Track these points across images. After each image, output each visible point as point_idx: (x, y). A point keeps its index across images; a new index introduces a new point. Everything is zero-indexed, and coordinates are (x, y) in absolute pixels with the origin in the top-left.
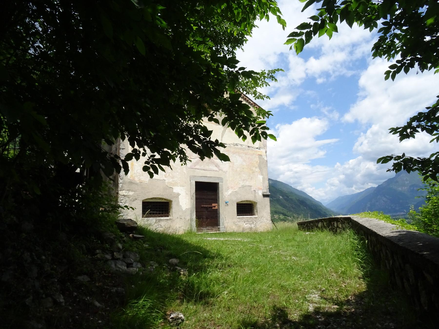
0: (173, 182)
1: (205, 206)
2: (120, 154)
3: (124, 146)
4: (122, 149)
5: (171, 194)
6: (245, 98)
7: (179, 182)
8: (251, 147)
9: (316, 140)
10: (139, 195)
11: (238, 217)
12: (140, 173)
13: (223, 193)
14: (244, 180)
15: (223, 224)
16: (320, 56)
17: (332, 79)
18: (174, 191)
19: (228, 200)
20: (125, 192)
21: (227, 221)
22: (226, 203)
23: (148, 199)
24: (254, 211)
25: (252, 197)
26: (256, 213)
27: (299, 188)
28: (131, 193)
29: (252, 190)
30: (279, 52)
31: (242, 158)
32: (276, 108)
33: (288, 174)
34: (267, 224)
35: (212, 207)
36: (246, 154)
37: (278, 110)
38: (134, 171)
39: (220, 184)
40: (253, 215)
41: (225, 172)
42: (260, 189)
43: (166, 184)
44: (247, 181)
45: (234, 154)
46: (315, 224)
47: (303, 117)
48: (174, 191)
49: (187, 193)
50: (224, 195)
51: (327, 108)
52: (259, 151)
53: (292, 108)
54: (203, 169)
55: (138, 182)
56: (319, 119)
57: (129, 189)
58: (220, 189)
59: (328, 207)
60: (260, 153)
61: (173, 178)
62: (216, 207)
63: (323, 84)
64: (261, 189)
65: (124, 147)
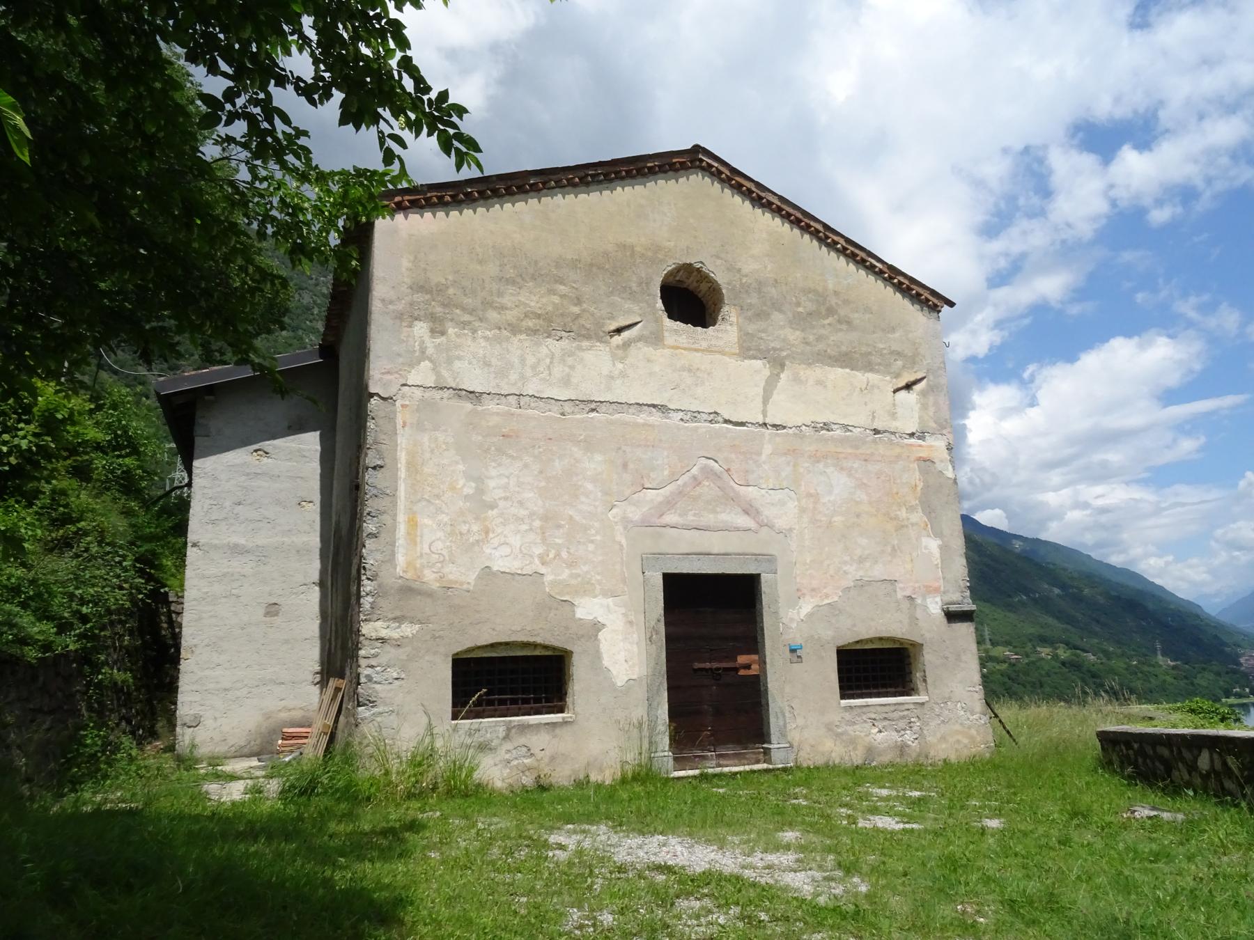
0: (573, 582)
1: (708, 665)
2: (367, 487)
3: (379, 459)
4: (374, 468)
5: (567, 628)
6: (852, 252)
7: (599, 577)
8: (885, 431)
9: (1165, 406)
10: (439, 637)
11: (844, 702)
12: (445, 552)
13: (776, 613)
14: (861, 560)
15: (783, 735)
16: (1155, 138)
17: (1204, 204)
18: (580, 613)
19: (799, 641)
20: (385, 625)
21: (800, 721)
22: (793, 651)
23: (479, 648)
24: (914, 679)
25: (901, 622)
26: (920, 685)
27: (1116, 560)
28: (408, 630)
29: (900, 595)
30: (1019, 146)
31: (850, 475)
32: (1023, 316)
33: (1074, 515)
34: (969, 728)
35: (736, 670)
36: (866, 460)
37: (1027, 321)
38: (418, 549)
39: (764, 577)
40: (908, 695)
41: (786, 533)
42: (931, 590)
43: (547, 590)
44: (876, 562)
45: (818, 462)
46: (1180, 752)
47: (1113, 336)
48: (580, 613)
49: (632, 618)
50: (784, 620)
51: (1193, 300)
52: (920, 446)
53: (1075, 310)
54: (694, 524)
55: (435, 586)
56: (1170, 337)
57: (398, 613)
58: (765, 599)
59: (1226, 619)
60: (924, 454)
61: (571, 564)
62: (755, 667)
63: (1171, 227)
64: (937, 590)
65: (379, 463)
